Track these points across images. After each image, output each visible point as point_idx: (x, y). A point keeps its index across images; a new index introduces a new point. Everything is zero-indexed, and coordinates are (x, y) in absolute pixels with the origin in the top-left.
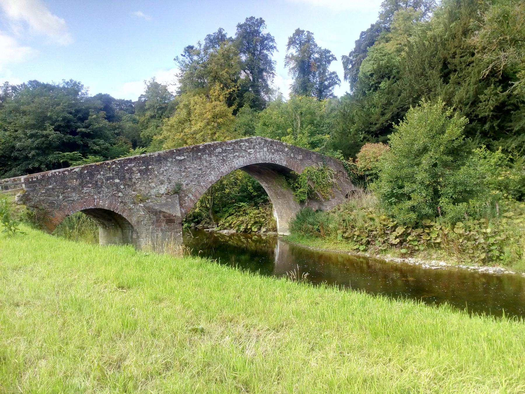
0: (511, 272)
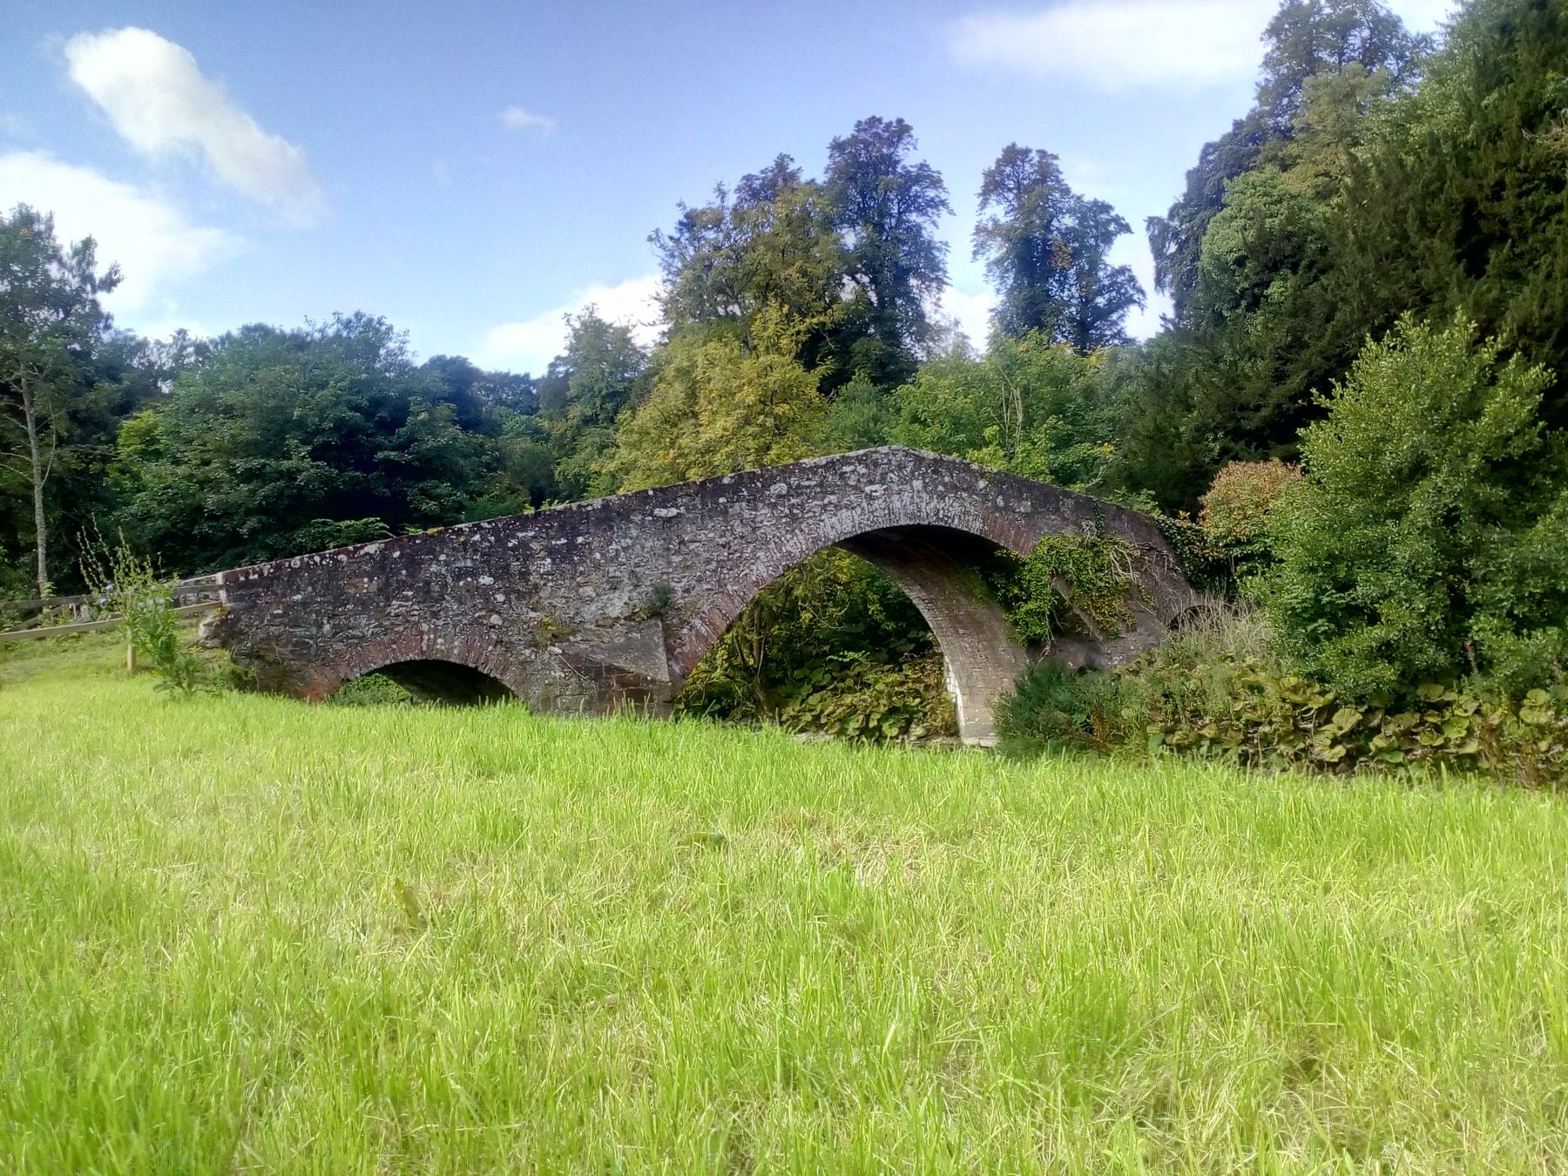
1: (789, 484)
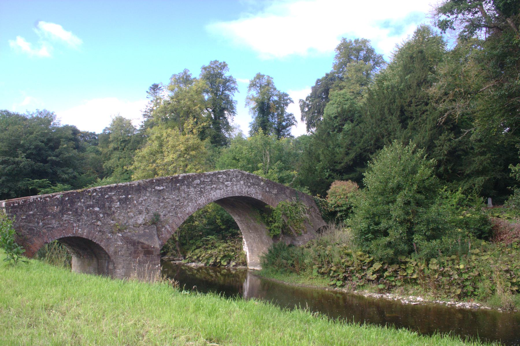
0: (485, 307)
1: (200, 180)
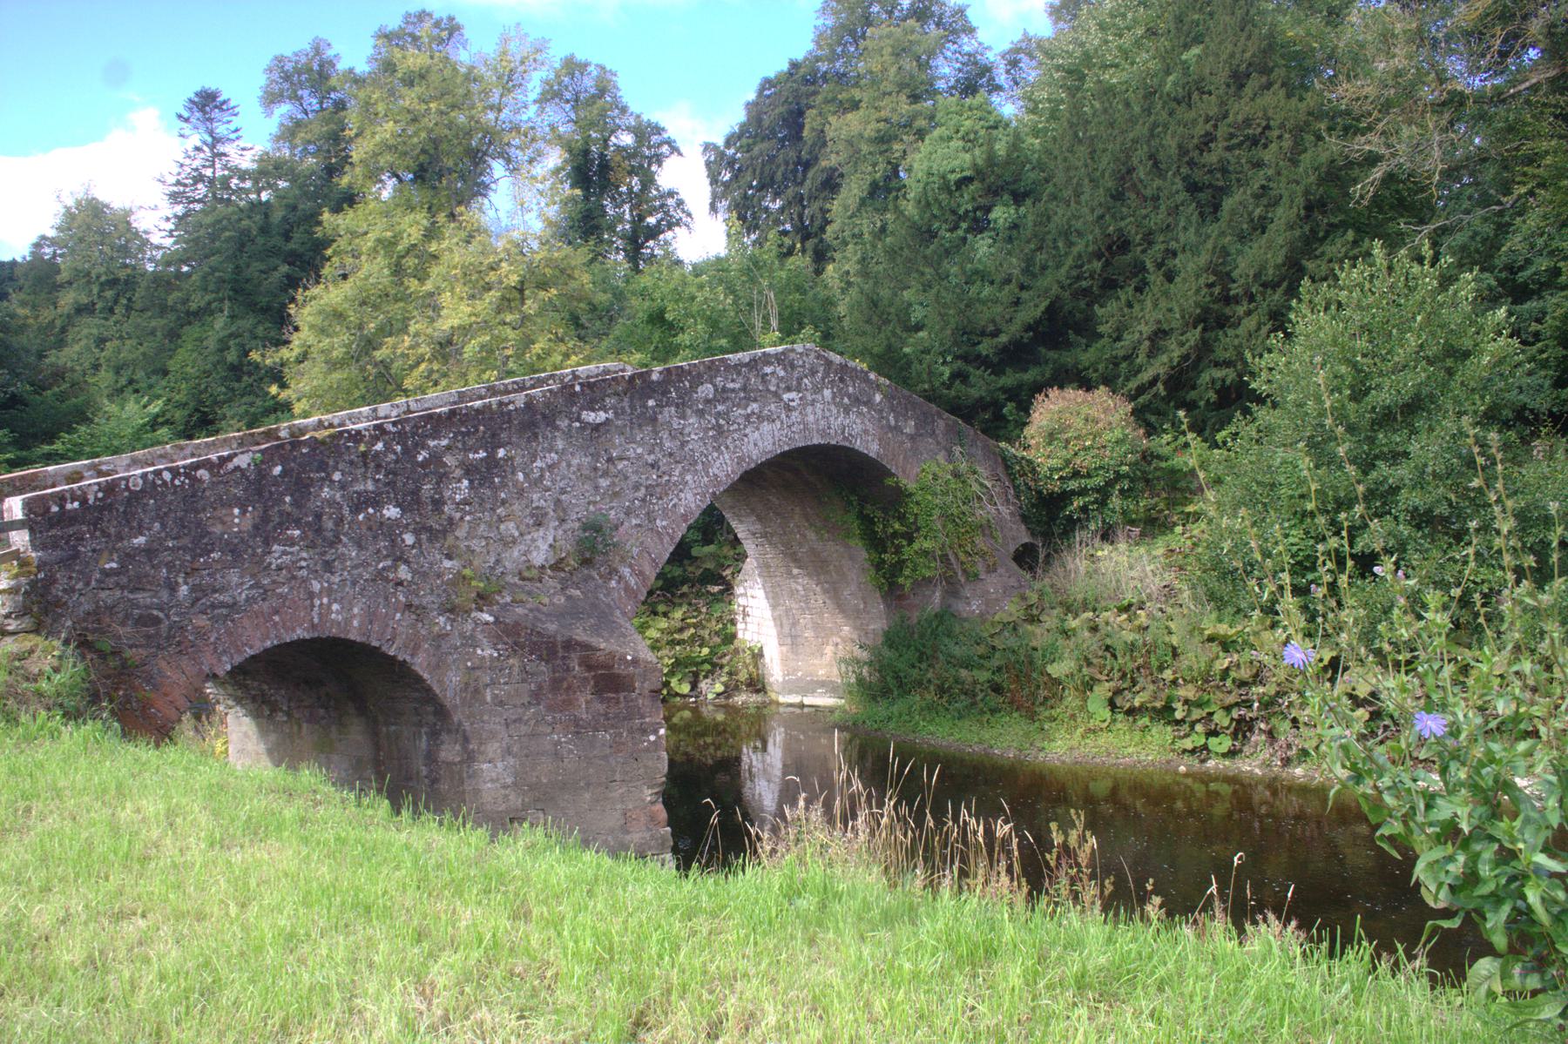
1: (715, 386)
